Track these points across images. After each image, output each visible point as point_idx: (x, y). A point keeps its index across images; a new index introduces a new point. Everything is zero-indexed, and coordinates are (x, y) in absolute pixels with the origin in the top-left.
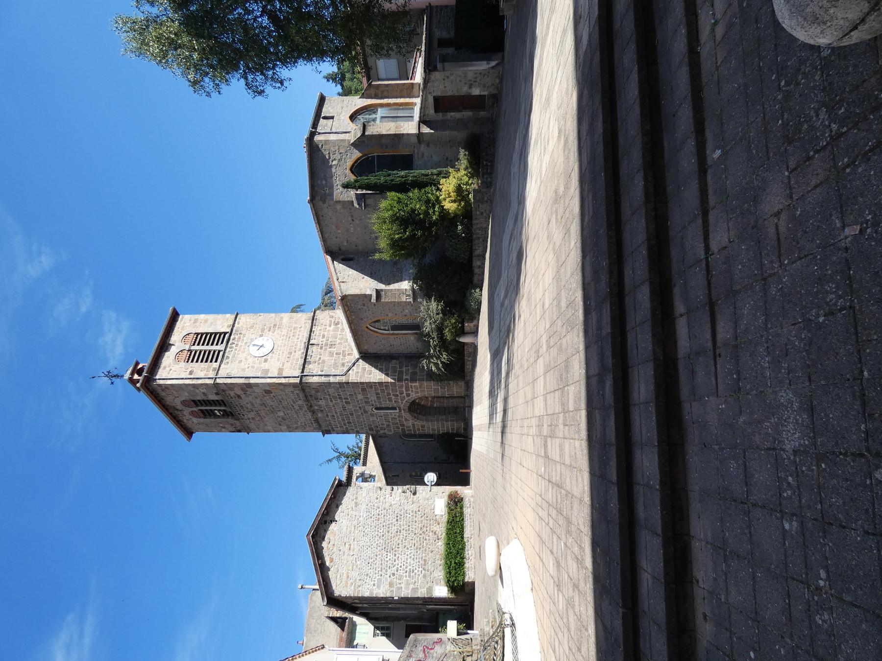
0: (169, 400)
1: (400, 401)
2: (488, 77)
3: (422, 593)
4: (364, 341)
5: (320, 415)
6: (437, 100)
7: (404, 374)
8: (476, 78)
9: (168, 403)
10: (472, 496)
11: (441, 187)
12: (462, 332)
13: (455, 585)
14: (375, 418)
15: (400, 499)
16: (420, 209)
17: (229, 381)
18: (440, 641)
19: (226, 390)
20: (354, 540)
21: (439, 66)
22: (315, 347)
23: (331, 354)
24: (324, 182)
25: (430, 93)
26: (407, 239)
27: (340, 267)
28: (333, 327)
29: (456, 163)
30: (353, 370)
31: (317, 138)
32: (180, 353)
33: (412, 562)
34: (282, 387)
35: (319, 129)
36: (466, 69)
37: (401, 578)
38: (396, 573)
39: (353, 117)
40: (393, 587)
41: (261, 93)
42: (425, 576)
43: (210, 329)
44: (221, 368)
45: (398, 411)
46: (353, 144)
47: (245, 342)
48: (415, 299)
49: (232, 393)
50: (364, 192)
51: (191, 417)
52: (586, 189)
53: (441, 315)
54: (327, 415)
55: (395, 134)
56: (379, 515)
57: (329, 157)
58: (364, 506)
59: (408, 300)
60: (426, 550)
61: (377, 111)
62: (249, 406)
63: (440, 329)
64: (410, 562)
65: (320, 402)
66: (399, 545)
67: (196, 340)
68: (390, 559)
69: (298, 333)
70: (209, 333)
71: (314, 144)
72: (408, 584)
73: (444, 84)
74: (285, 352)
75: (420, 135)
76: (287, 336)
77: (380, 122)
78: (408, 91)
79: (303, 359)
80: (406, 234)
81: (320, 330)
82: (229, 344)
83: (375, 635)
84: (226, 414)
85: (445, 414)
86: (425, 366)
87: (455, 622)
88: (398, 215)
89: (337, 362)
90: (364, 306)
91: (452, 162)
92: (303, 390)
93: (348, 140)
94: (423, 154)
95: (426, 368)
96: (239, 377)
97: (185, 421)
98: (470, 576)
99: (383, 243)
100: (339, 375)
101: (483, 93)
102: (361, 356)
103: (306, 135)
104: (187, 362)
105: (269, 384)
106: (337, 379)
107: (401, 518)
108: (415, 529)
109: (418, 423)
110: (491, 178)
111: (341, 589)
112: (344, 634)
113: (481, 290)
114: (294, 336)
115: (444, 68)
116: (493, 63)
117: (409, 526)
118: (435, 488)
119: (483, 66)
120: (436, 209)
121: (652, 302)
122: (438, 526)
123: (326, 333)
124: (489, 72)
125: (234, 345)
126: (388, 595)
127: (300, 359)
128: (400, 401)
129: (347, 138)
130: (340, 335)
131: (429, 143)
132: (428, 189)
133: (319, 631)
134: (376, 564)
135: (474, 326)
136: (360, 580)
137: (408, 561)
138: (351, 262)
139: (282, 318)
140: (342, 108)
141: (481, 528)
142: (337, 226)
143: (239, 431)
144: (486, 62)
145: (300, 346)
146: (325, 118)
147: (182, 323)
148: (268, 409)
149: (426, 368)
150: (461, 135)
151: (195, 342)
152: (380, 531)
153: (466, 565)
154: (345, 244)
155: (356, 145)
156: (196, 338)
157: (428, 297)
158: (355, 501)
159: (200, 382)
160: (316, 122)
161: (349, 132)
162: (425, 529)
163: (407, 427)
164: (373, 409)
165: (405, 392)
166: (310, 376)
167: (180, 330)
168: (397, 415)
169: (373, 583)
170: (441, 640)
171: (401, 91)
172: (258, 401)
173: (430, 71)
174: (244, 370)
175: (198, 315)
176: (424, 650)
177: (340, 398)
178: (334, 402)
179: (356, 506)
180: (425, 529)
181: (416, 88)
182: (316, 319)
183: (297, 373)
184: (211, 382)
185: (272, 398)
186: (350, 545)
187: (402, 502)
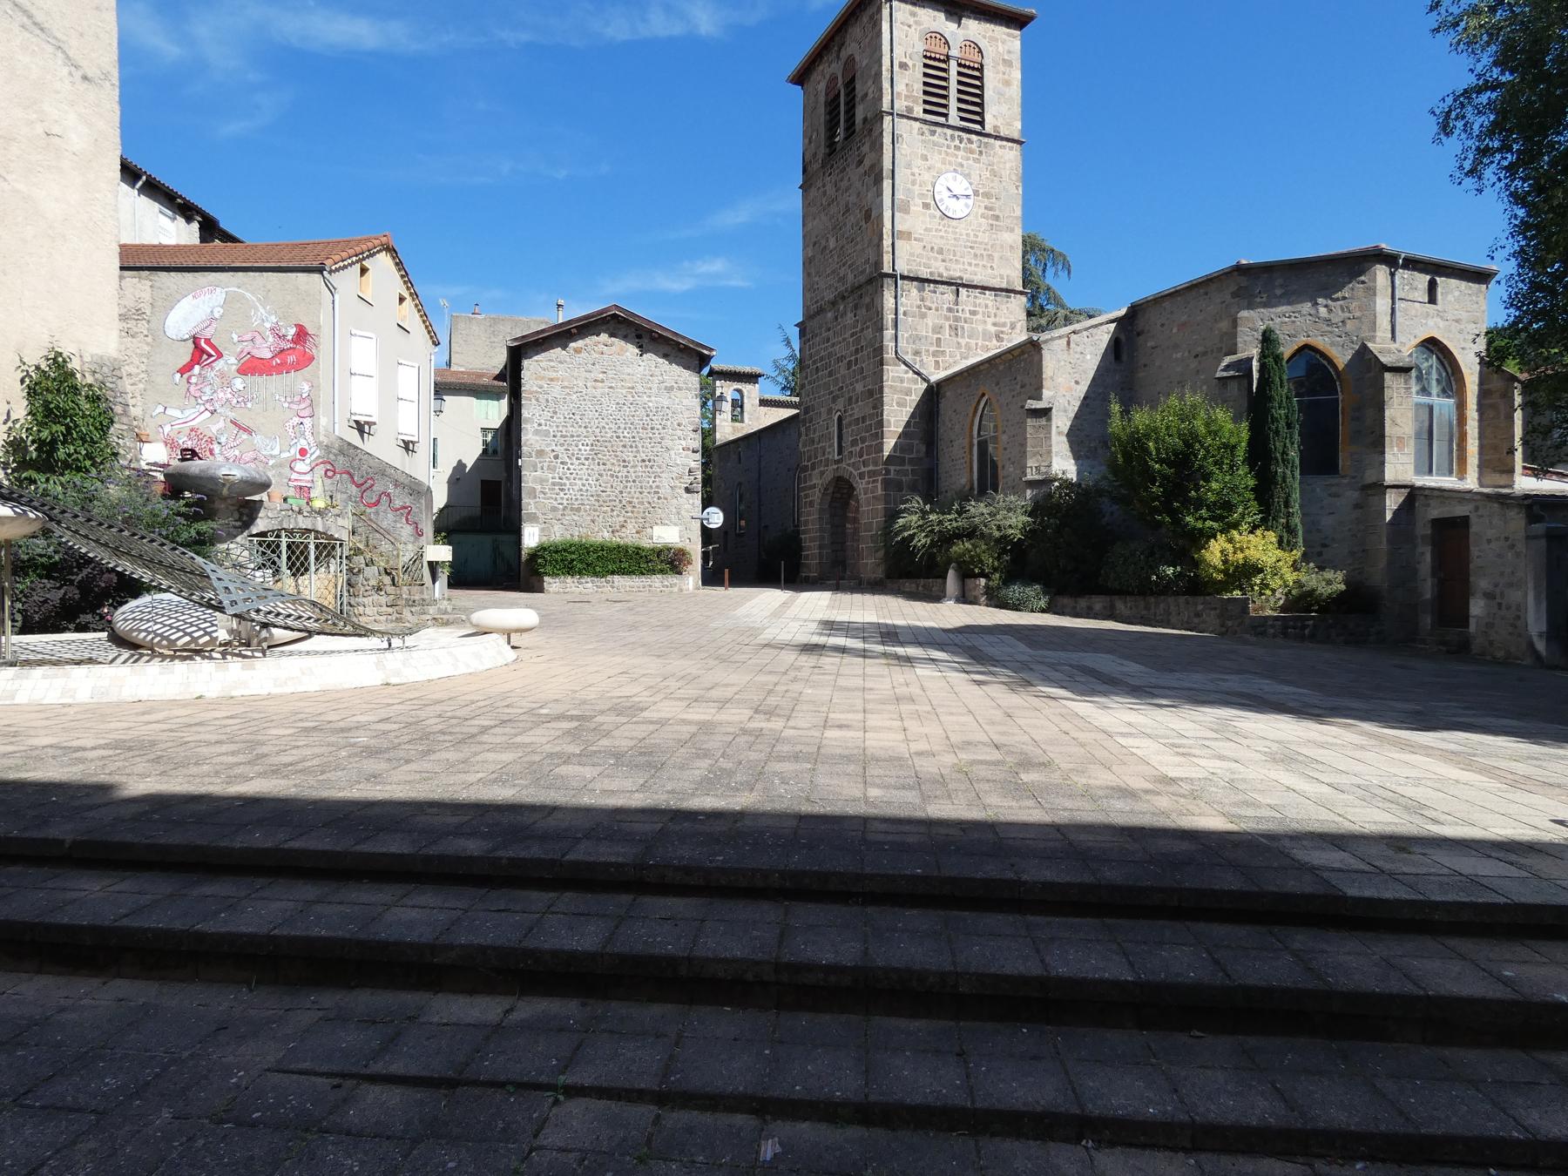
0: (856, 31)
1: (853, 460)
2: (1510, 634)
3: (529, 505)
4: (959, 391)
5: (830, 315)
6: (1464, 522)
7: (898, 468)
8: (1508, 608)
9: (850, 30)
10: (681, 590)
11: (1258, 532)
12: (966, 575)
13: (539, 561)
14: (824, 416)
15: (678, 465)
16: (1209, 490)
17: (887, 140)
18: (419, 533)
19: (870, 136)
20: (611, 387)
21: (1539, 528)
22: (952, 297)
23: (938, 329)
24: (1278, 292)
25: (1477, 509)
26: (1147, 469)
27: (1104, 336)
28: (993, 329)
29: (1312, 565)
30: (906, 372)
31: (1381, 273)
32: (943, 40)
33: (576, 488)
34: (876, 241)
35: (1403, 275)
36: (1531, 585)
37: (552, 469)
38: (559, 461)
39: (1432, 345)
40: (537, 457)
41: (1445, 129)
42: (554, 509)
43: (991, 93)
44: (913, 122)
45: (836, 457)
46: (1364, 348)
47: (964, 163)
48: (1032, 484)
49: (866, 148)
50: (1256, 375)
51: (828, 77)
52: (952, 831)
53: (997, 534)
54: (829, 330)
55: (1383, 436)
56: (652, 429)
57: (1338, 299)
58: (666, 403)
59: (1029, 470)
60: (595, 510)
61: (1449, 397)
62: (845, 184)
63: (971, 533)
64: (576, 484)
65: (850, 315)
66: (604, 464)
67: (969, 67)
68: (580, 450)
69: (981, 263)
70: (983, 91)
71: (1366, 265)
72: (542, 481)
73: (1498, 539)
74: (943, 241)
75: (1380, 488)
76: (976, 242)
77: (1417, 405)
78: (1496, 460)
79: (929, 277)
80: (1156, 463)
81: (986, 306)
82: (961, 133)
83: (484, 430)
84: (831, 145)
85: (832, 543)
86: (907, 506)
87: (450, 558)
88: (1197, 446)
89: (923, 340)
90: (1022, 387)
91: (1317, 555)
92: (870, 281)
93: (1374, 337)
94: (1336, 495)
95: (903, 507)
96: (893, 157)
97: (821, 68)
98: (553, 584)
99: (1141, 418)
100: (896, 347)
101: (1472, 622)
102: (932, 387)
103: (1385, 246)
104: (925, 57)
105: (880, 216)
106: (889, 344)
107: (646, 466)
108: (630, 493)
109: (816, 495)
110: (1274, 636)
111: (533, 369)
112: (485, 381)
113: (1043, 611)
114: (976, 255)
115: (1535, 537)
116: (1541, 646)
117: (634, 481)
118: (697, 526)
119: (1535, 623)
120: (1209, 523)
121: (555, 953)
122: (634, 531)
123: (979, 317)
124: (1520, 635)
125: (957, 142)
126: (524, 449)
127: (928, 271)
128: (853, 460)
129: (1379, 334)
130: (977, 344)
131: (1361, 508)
132: (1254, 506)
133: (493, 339)
134: (573, 426)
135: (976, 597)
136: (547, 400)
137: (577, 481)
138: (1112, 358)
139: (1012, 230)
140: (1457, 321)
141: (617, 604)
142: (1184, 325)
143: (805, 171)
144: (1544, 629)
145: (955, 270)
146: (1432, 286)
147: (1004, 37)
148: (841, 218)
149: (903, 507)
150: (1378, 574)
151: (964, 66)
152: (625, 432)
153: (569, 579)
154: (1149, 344)
155: (1364, 356)
156: (973, 69)
157: (1035, 510)
158: (676, 385)
159: (886, 85)
160: (1421, 266)
161: (1393, 337)
162: (629, 509)
163: (810, 475)
164: (839, 413)
165: (866, 469)
166: (896, 292)
167: (990, 33)
168: (830, 457)
169: (543, 422)
170: (419, 535)
171: (1495, 448)
172: (853, 199)
173: (1529, 507)
174: (909, 166)
175: (1019, 65)
176: (406, 508)
177: (857, 351)
178: (851, 340)
179: (666, 388)
180: (629, 509)
181: (1502, 480)
182: (1010, 297)
183: (902, 268)
184: (886, 106)
185: (858, 224)
186: (603, 381)
187: (674, 469)
